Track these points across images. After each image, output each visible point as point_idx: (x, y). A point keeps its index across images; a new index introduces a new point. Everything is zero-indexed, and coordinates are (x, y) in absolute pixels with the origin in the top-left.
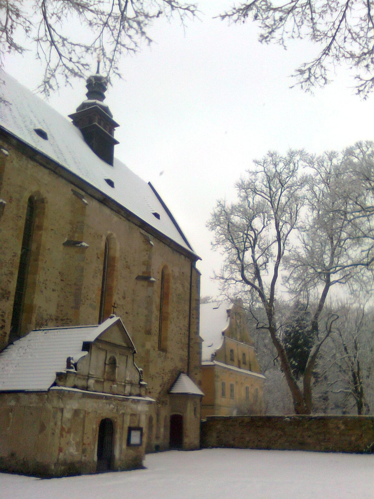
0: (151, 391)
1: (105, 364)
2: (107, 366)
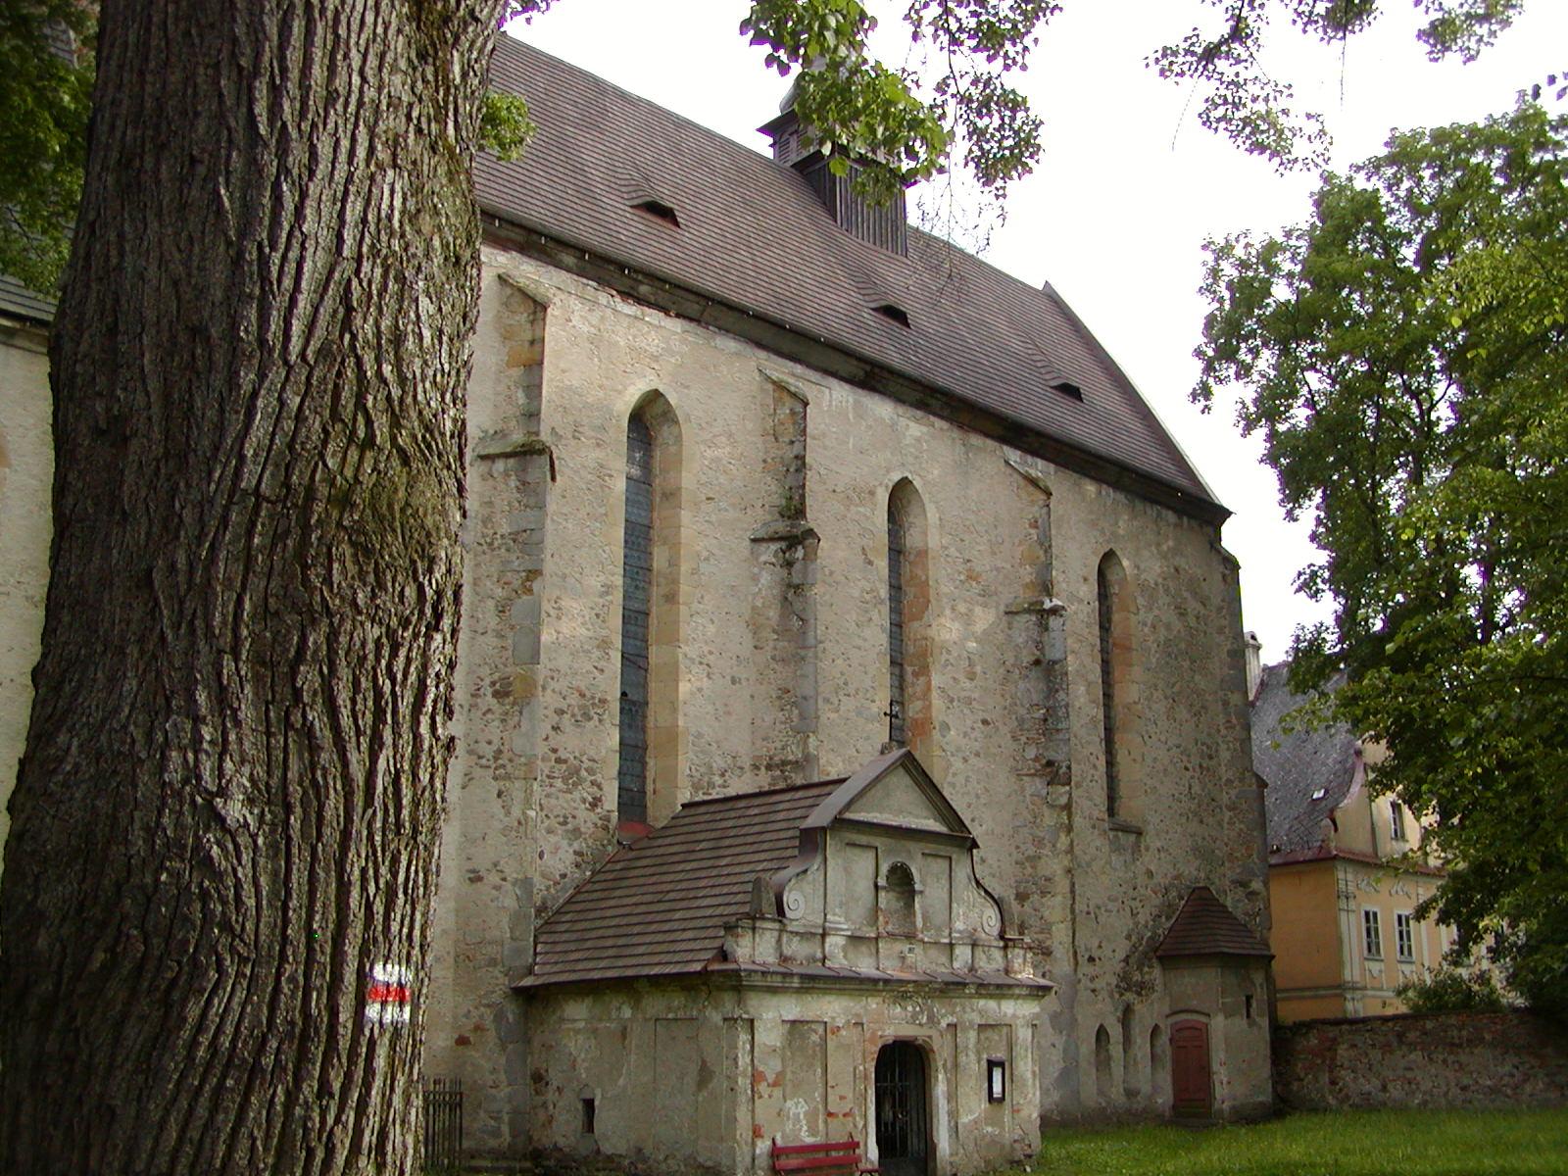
0: (1095, 955)
1: (876, 886)
2: (882, 894)
